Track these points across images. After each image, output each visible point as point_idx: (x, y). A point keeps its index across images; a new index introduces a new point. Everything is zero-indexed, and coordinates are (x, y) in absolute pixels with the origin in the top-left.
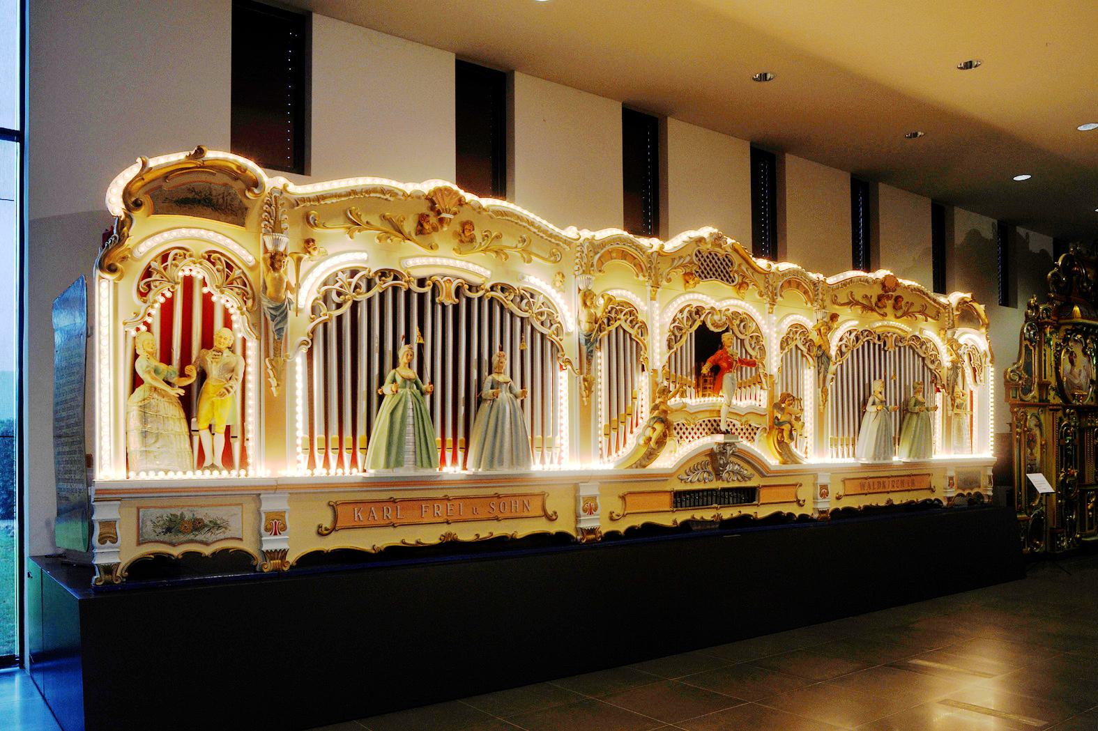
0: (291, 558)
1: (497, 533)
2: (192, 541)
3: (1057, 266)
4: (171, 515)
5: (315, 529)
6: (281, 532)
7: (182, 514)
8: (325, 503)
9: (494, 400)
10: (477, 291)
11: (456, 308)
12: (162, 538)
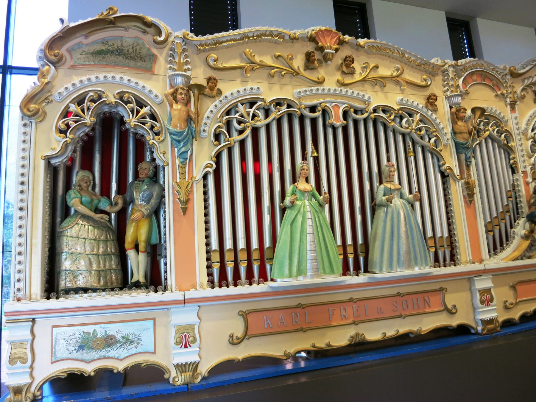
0: (204, 369)
1: (402, 330)
4: (84, 332)
7: (95, 331)
9: (388, 206)
10: (363, 114)
11: (345, 129)
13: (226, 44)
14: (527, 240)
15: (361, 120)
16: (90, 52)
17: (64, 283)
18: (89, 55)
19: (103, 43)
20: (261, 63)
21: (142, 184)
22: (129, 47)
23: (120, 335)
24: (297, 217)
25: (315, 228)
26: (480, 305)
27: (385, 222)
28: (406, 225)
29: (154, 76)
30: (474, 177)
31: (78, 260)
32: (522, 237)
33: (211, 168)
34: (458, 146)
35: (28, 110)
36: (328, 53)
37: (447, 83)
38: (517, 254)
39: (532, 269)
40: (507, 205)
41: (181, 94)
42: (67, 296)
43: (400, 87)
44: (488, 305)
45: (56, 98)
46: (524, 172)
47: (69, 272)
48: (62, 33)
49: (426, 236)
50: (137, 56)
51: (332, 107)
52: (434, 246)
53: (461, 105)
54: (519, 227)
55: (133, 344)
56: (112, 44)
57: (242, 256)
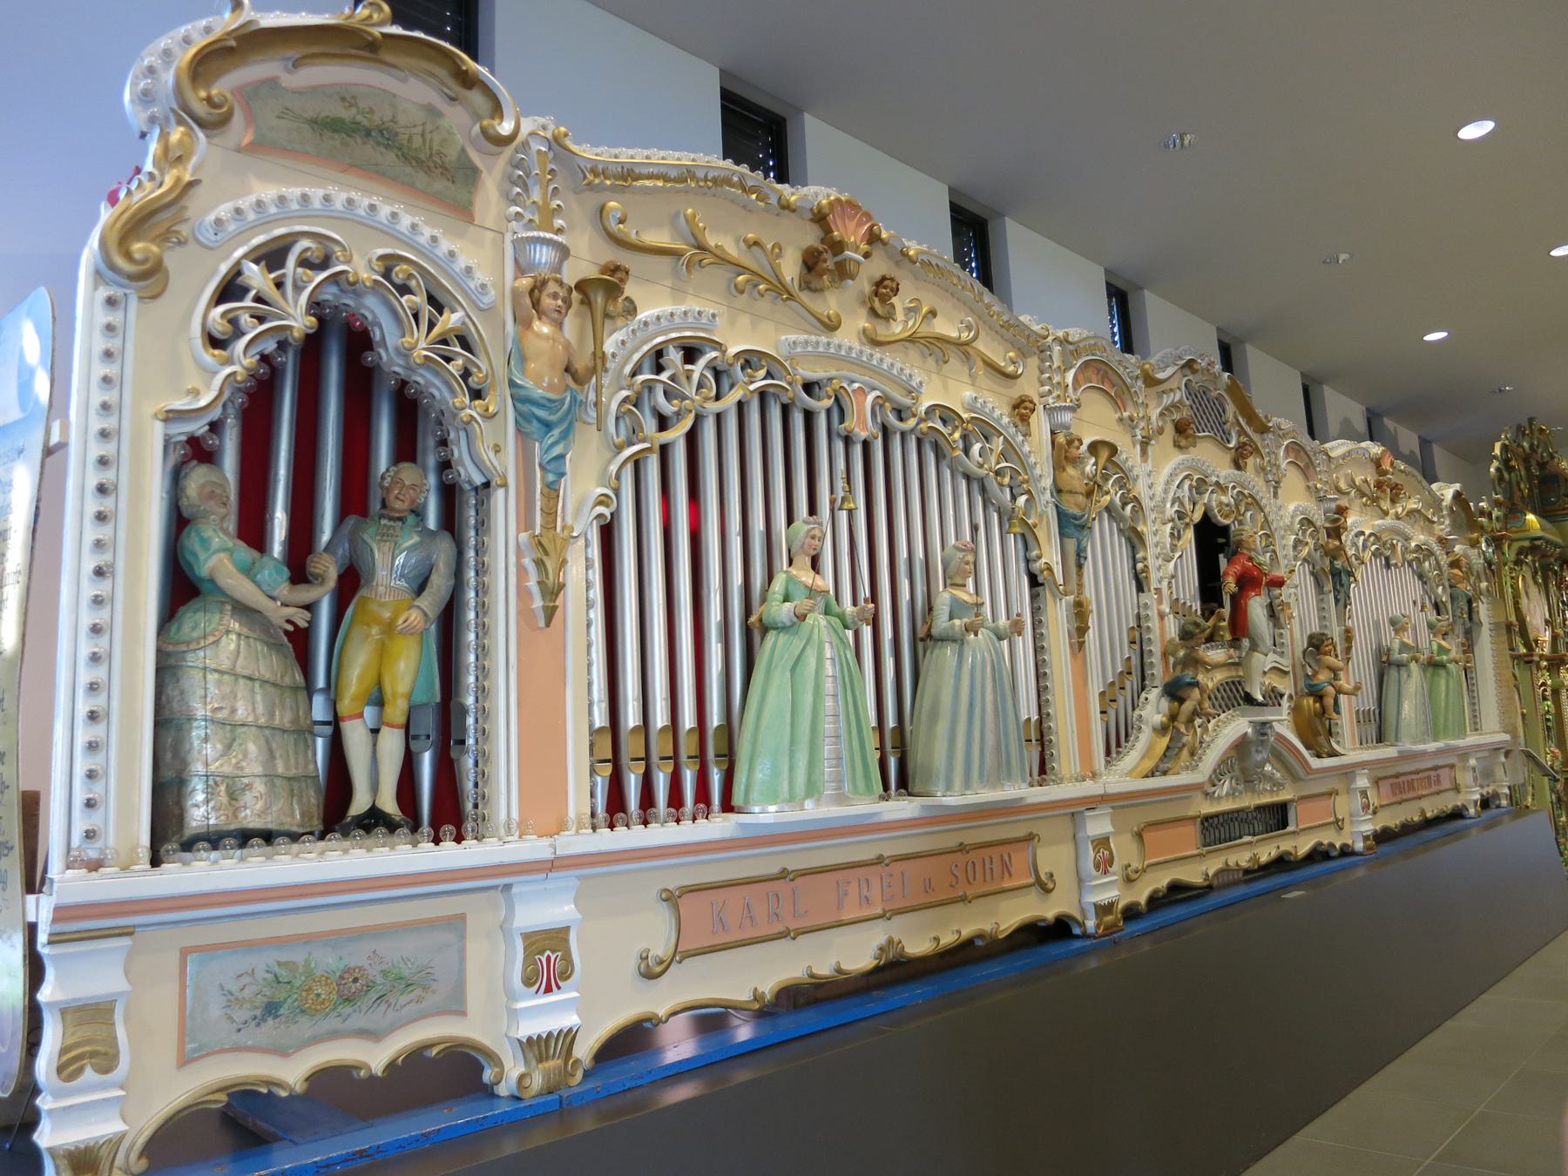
1: (967, 931)
2: (334, 1035)
3: (1495, 457)
4: (279, 964)
5: (632, 964)
6: (560, 983)
7: (307, 962)
8: (654, 892)
12: (246, 1038)
13: (648, 183)
14: (1164, 735)
15: (895, 432)
16: (305, 116)
17: (200, 812)
18: (302, 125)
19: (343, 99)
20: (718, 252)
21: (402, 528)
22: (414, 131)
23: (379, 968)
24: (805, 654)
25: (839, 681)
26: (1094, 872)
27: (958, 677)
28: (994, 687)
29: (472, 228)
30: (1089, 593)
31: (240, 745)
32: (1155, 729)
33: (607, 506)
34: (1062, 516)
35: (128, 256)
36: (851, 259)
37: (1049, 378)
38: (1149, 764)
39: (1169, 797)
40: (1129, 658)
41: (555, 296)
42: (188, 855)
43: (970, 370)
44: (1106, 872)
45: (205, 233)
46: (1158, 591)
47: (218, 779)
48: (236, 39)
49: (681, 724)
50: (435, 162)
51: (854, 391)
52: (726, 752)
53: (1071, 430)
54: (1149, 707)
55: (412, 991)
56: (367, 110)
57: (660, 747)
